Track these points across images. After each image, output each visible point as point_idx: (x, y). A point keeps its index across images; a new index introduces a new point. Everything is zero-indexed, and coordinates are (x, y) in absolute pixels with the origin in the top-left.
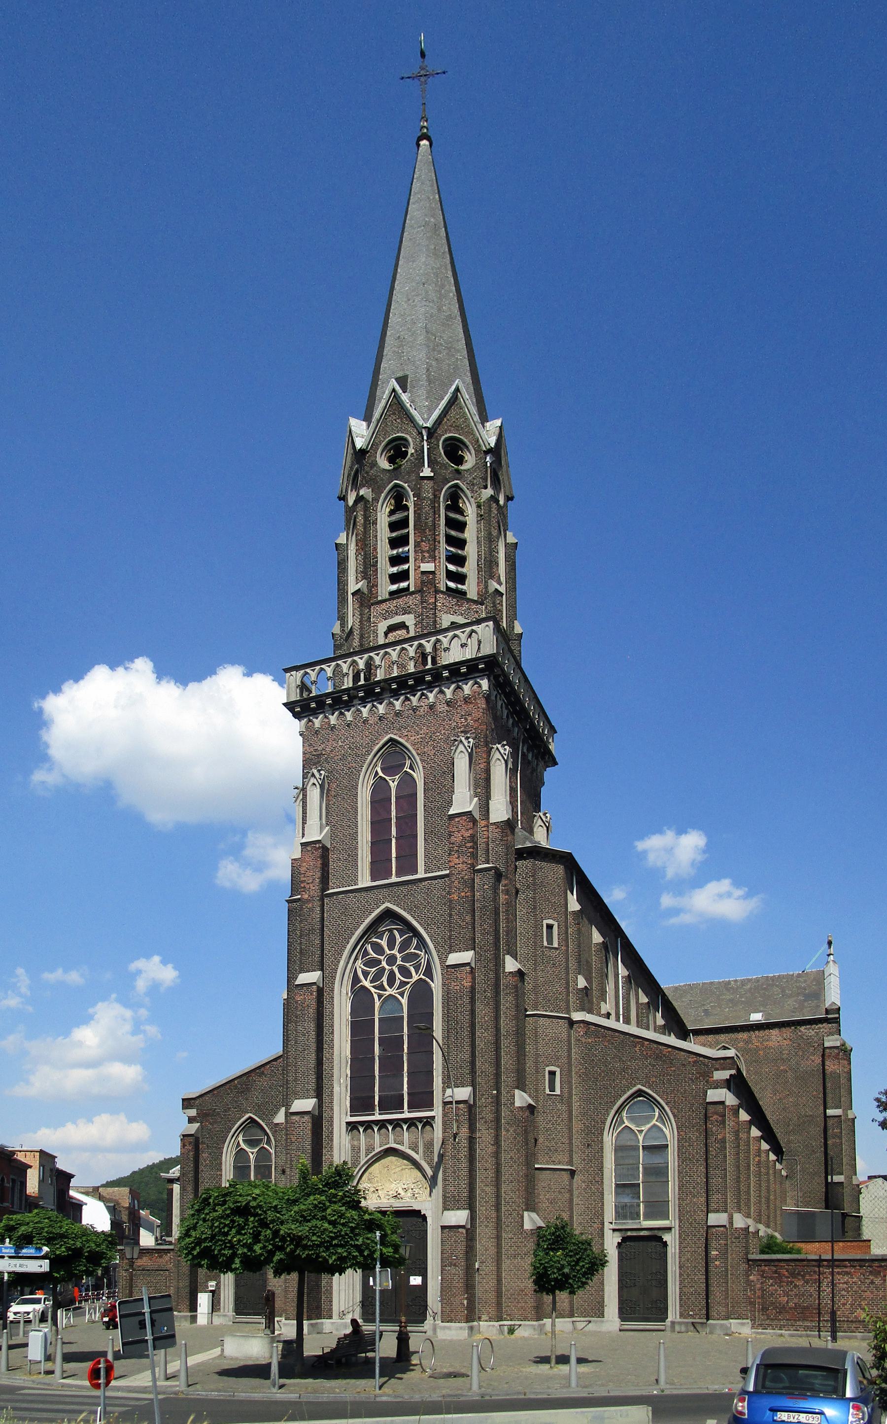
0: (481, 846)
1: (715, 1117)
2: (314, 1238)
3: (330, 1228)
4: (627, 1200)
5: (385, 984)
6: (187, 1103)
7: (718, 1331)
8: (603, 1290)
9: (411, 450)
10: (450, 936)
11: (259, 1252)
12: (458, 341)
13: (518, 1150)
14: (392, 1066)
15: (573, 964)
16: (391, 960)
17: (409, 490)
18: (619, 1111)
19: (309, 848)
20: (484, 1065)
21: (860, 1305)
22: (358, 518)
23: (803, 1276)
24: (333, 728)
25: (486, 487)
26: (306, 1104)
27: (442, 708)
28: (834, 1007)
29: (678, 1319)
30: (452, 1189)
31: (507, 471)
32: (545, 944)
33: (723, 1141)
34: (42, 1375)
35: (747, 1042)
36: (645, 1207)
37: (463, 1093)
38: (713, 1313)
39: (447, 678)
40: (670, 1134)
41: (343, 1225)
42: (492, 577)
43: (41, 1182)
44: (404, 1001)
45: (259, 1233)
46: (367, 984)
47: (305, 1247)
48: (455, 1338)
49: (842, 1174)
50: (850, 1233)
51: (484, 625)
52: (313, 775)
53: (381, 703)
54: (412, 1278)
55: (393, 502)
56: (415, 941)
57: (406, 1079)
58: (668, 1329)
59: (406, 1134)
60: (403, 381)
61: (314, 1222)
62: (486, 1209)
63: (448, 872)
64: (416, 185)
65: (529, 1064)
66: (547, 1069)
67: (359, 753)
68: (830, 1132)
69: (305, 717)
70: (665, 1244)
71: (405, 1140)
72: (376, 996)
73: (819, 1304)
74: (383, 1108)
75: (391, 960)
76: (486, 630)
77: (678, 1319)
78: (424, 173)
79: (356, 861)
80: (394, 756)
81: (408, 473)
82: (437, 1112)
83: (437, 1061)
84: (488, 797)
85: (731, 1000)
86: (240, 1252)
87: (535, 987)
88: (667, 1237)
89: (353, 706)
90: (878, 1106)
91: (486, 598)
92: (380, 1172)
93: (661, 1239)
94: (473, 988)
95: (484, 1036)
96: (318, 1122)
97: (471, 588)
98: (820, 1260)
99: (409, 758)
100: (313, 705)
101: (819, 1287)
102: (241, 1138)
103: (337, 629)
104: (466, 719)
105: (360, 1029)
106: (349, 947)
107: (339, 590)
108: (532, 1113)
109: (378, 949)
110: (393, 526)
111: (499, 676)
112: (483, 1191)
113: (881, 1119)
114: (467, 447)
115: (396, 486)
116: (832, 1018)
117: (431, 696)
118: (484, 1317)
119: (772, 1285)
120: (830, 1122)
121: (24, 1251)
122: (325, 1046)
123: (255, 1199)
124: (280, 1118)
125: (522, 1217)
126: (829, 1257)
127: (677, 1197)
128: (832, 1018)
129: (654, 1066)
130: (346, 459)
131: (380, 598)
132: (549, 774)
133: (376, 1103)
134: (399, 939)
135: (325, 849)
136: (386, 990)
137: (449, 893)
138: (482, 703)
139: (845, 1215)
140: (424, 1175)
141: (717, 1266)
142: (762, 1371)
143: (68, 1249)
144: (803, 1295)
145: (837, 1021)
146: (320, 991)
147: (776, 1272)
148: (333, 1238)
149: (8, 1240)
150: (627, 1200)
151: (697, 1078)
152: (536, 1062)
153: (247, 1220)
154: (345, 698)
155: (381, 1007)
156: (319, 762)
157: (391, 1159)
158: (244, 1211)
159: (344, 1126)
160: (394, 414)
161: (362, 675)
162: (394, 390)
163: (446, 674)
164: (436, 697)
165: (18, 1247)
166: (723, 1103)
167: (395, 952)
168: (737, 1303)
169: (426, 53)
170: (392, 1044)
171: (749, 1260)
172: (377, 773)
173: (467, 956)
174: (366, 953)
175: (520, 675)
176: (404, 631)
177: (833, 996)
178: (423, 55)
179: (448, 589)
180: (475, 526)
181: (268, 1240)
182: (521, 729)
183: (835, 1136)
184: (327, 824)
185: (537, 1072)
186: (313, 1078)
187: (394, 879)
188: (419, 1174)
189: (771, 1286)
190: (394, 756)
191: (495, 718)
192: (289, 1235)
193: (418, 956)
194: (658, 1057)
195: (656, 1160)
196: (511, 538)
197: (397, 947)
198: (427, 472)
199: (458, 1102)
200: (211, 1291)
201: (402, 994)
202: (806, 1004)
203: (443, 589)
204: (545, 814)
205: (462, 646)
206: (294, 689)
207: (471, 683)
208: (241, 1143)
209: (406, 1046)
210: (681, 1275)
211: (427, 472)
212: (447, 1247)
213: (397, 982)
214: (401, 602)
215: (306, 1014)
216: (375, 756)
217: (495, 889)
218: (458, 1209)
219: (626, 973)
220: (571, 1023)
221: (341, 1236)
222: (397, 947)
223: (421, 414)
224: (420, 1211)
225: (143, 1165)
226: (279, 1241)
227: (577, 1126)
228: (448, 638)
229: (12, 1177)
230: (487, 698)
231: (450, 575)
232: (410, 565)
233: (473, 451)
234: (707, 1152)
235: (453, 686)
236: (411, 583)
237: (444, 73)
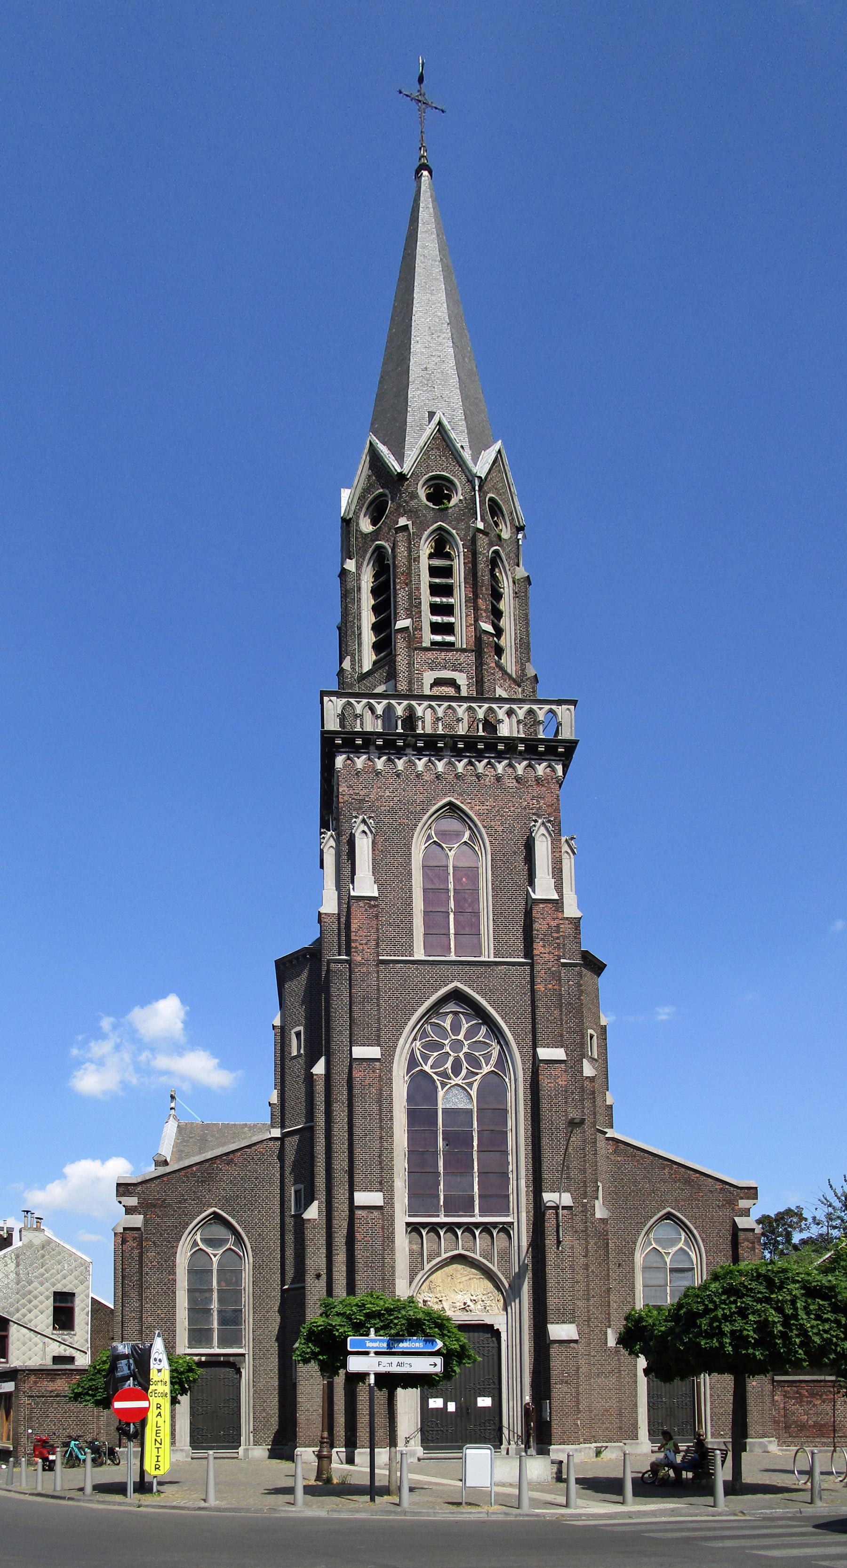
1: (746, 1243)
8: (636, 1412)
13: (600, 1264)
18: (647, 1233)
19: (361, 904)
24: (378, 773)
27: (511, 783)
39: (521, 752)
46: (427, 1068)
51: (564, 707)
53: (439, 760)
57: (476, 1180)
71: (478, 1247)
73: (834, 1421)
74: (450, 1209)
75: (457, 1045)
89: (406, 755)
92: (443, 1281)
99: (470, 828)
100: (359, 742)
101: (834, 1406)
102: (198, 1237)
110: (434, 571)
114: (503, 516)
119: (794, 1405)
121: (401, 1345)
125: (606, 1333)
129: (683, 1190)
131: (424, 645)
136: (450, 1079)
140: (498, 1286)
141: (754, 1387)
147: (797, 1392)
151: (723, 1205)
157: (457, 1268)
161: (399, 723)
166: (753, 1230)
169: (425, 81)
170: (458, 1140)
174: (425, 1034)
178: (421, 80)
188: (489, 1285)
193: (490, 1045)
194: (688, 1182)
201: (470, 1085)
207: (545, 764)
209: (475, 1143)
213: (464, 1072)
216: (431, 817)
218: (564, 1322)
224: (492, 1326)
235: (525, 763)
237: (443, 111)
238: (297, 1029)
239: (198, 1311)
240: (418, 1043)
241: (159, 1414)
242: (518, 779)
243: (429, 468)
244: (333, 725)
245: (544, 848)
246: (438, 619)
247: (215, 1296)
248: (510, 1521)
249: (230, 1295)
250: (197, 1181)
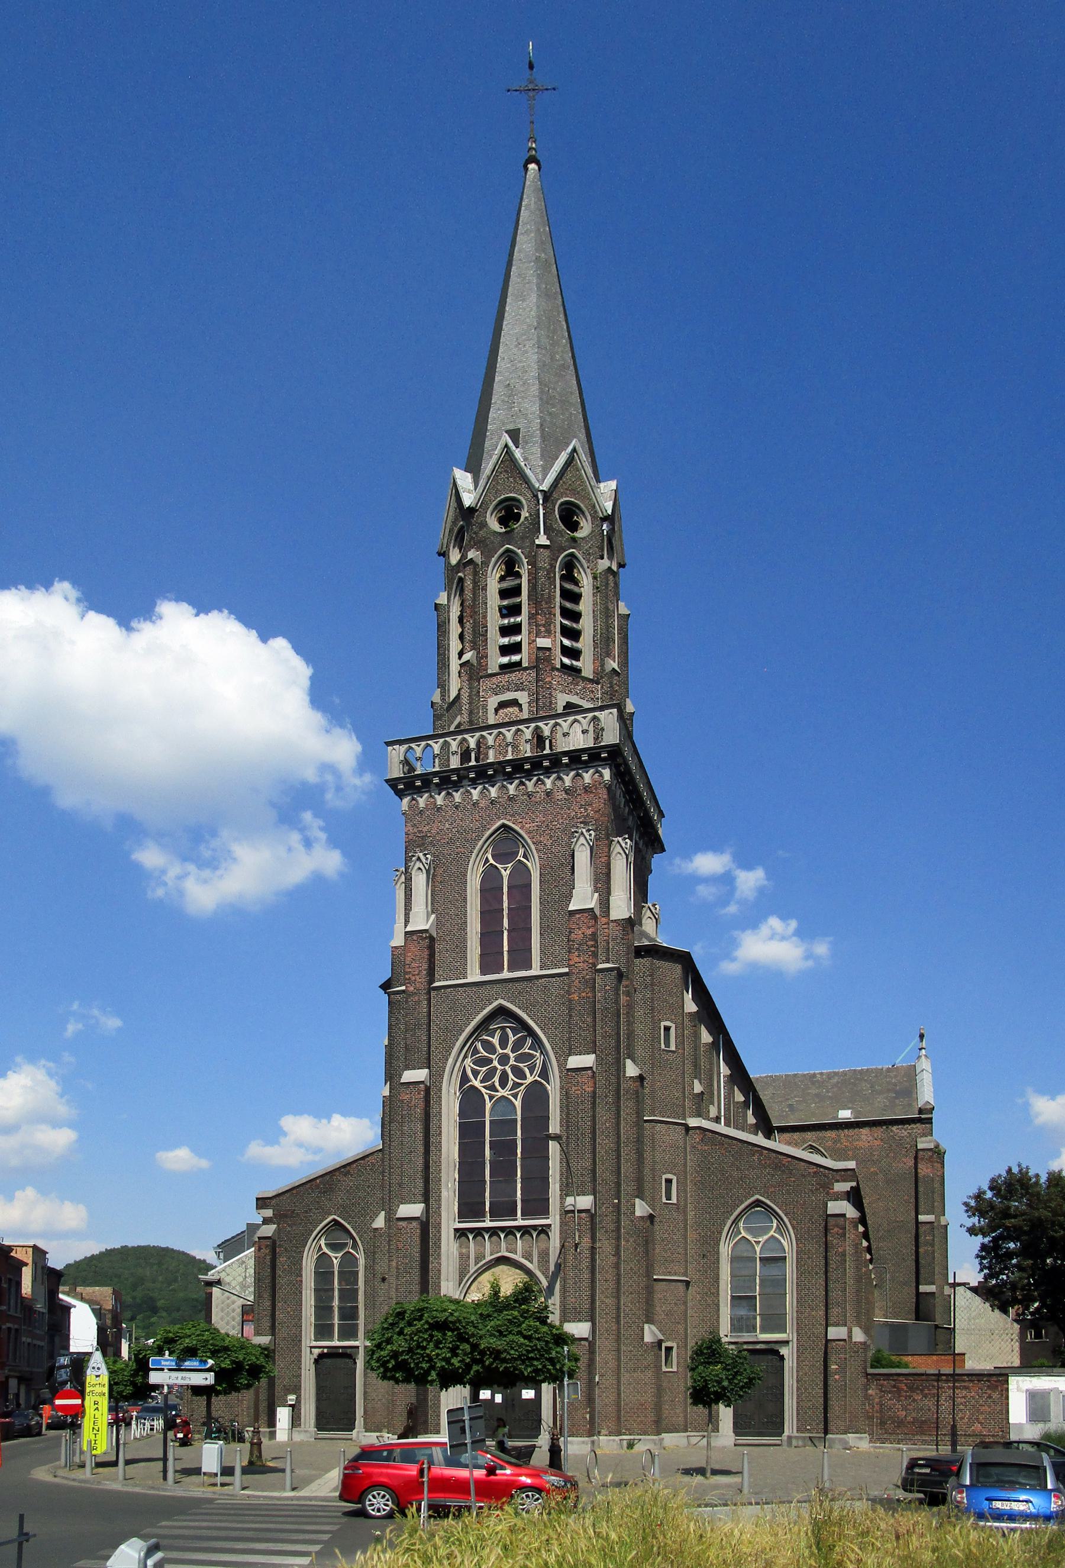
0: (602, 944)
1: (836, 1229)
2: (512, 1352)
3: (526, 1342)
4: (743, 1312)
5: (497, 1084)
6: (262, 1203)
7: (838, 1446)
9: (524, 514)
10: (569, 1039)
11: (457, 1365)
12: (571, 393)
14: (504, 1170)
15: (689, 1068)
16: (504, 1060)
17: (523, 557)
18: (736, 1221)
19: (415, 938)
20: (604, 1172)
21: (977, 1419)
22: (461, 580)
23: (922, 1391)
24: (439, 809)
25: (602, 558)
26: (413, 1209)
27: (561, 795)
28: (929, 1107)
29: (795, 1434)
30: (573, 1300)
31: (621, 536)
32: (663, 1046)
33: (843, 1254)
34: (219, 1488)
35: (835, 1142)
36: (762, 1320)
37: (585, 1202)
38: (832, 1426)
39: (567, 765)
40: (788, 1245)
41: (538, 1339)
42: (608, 655)
43: (34, 1280)
44: (518, 1103)
45: (458, 1347)
46: (477, 1083)
47: (504, 1360)
48: (577, 1452)
49: (933, 1284)
50: (940, 1346)
52: (419, 859)
53: (493, 786)
54: (524, 1392)
55: (503, 567)
56: (529, 1041)
57: (519, 1186)
58: (785, 1443)
59: (519, 1242)
60: (514, 434)
61: (511, 1337)
62: (606, 1322)
63: (566, 970)
64: (524, 213)
65: (647, 1171)
66: (664, 1177)
67: (469, 837)
68: (922, 1239)
69: (409, 795)
70: (782, 1358)
72: (487, 1097)
73: (938, 1418)
74: (495, 1214)
75: (504, 1060)
76: (609, 718)
77: (795, 1434)
78: (531, 202)
79: (465, 952)
80: (506, 843)
81: (522, 538)
82: (553, 1220)
83: (554, 1167)
84: (609, 893)
85: (817, 1095)
86: (438, 1365)
87: (653, 1092)
88: (784, 1351)
90: (967, 1211)
91: (602, 677)
93: (777, 1352)
94: (594, 1092)
95: (605, 1143)
96: (426, 1227)
97: (586, 665)
98: (939, 1375)
99: (523, 846)
100: (418, 783)
102: (322, 1242)
103: (436, 697)
104: (586, 810)
105: (470, 1132)
106: (458, 1044)
107: (439, 654)
108: (652, 1222)
109: (489, 1047)
110: (504, 594)
111: (620, 765)
112: (602, 1302)
113: (969, 1224)
114: (583, 513)
115: (508, 550)
116: (924, 1119)
117: (549, 783)
118: (603, 1432)
119: (890, 1399)
120: (922, 1229)
121: (186, 1363)
122: (432, 1148)
123: (451, 1314)
124: (380, 1222)
125: (643, 1330)
126: (950, 1371)
127: (795, 1309)
128: (924, 1119)
129: (773, 1175)
130: (447, 514)
131: (490, 671)
132: (656, 860)
133: (487, 1209)
134: (512, 1039)
135: (432, 939)
137: (569, 993)
138: (604, 794)
139: (937, 1327)
142: (974, 1469)
143: (233, 1362)
144: (922, 1409)
145: (929, 1121)
146: (428, 1090)
147: (894, 1386)
148: (528, 1352)
149: (167, 1353)
150: (743, 1312)
151: (817, 1189)
152: (653, 1170)
153: (445, 1334)
154: (455, 778)
155: (492, 1109)
156: (423, 844)
158: (442, 1326)
159: (452, 1232)
160: (506, 471)
162: (506, 446)
163: (565, 760)
164: (553, 783)
165: (180, 1360)
166: (844, 1215)
167: (508, 1051)
168: (855, 1417)
170: (504, 1148)
171: (868, 1375)
172: (487, 860)
173: (587, 1060)
174: (476, 1051)
175: (636, 760)
176: (517, 709)
177: (926, 1094)
178: (531, 67)
179: (563, 665)
180: (591, 599)
181: (465, 1354)
182: (635, 817)
183: (927, 1243)
184: (433, 912)
185: (654, 1180)
186: (420, 1183)
187: (506, 974)
189: (889, 1400)
190: (506, 843)
191: (615, 808)
192: (489, 1348)
193: (533, 1056)
194: (777, 1167)
195: (773, 1271)
196: (623, 609)
197: (510, 1046)
198: (542, 540)
199: (580, 1211)
200: (290, 1406)
201: (515, 1096)
202: (897, 1101)
203: (558, 666)
204: (654, 905)
205: (583, 732)
206: (397, 765)
207: (592, 771)
208: (323, 1246)
210: (798, 1389)
211: (542, 540)
213: (510, 1083)
214: (514, 677)
215: (407, 1116)
217: (617, 990)
218: (580, 1321)
219: (729, 1072)
220: (687, 1129)
221: (537, 1349)
222: (510, 1046)
223: (536, 475)
225: (79, 1257)
226: (478, 1353)
227: (691, 1235)
228: (569, 722)
229: (9, 1276)
230: (609, 789)
231: (566, 651)
232: (523, 638)
233: (589, 518)
234: (827, 1264)
235: (572, 773)
236: (523, 657)
239: (323, 1309)
240: (468, 1061)
241: (97, 1409)
242: (567, 791)
243: (498, 492)
244: (397, 772)
245: (584, 858)
246: (505, 641)
247: (336, 1293)
248: (138, 1494)
249: (349, 1295)
250: (320, 1192)
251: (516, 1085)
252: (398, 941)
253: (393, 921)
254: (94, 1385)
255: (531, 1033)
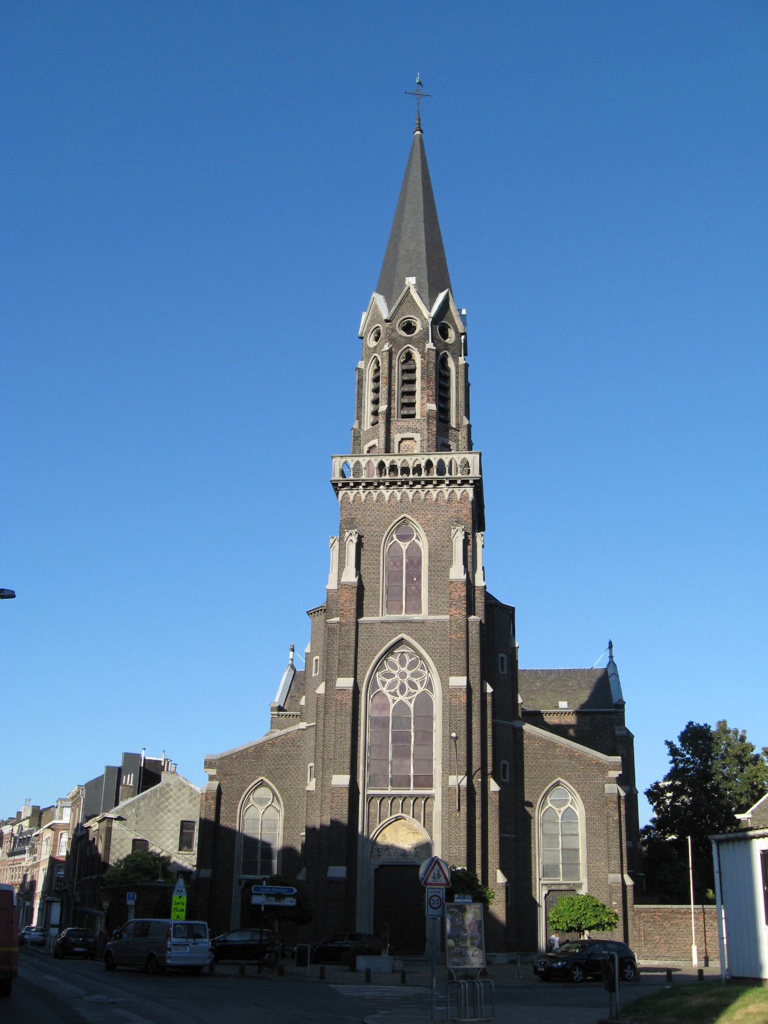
5: (398, 692)
6: (208, 764)
16: (403, 675)
44: (411, 706)
125: (496, 873)
197: (398, 666)
201: (410, 701)
209: (413, 740)
212: (610, 946)
238: (317, 657)
251: (410, 694)
252: (332, 585)
253: (327, 572)
254: (178, 904)
255: (422, 658)
